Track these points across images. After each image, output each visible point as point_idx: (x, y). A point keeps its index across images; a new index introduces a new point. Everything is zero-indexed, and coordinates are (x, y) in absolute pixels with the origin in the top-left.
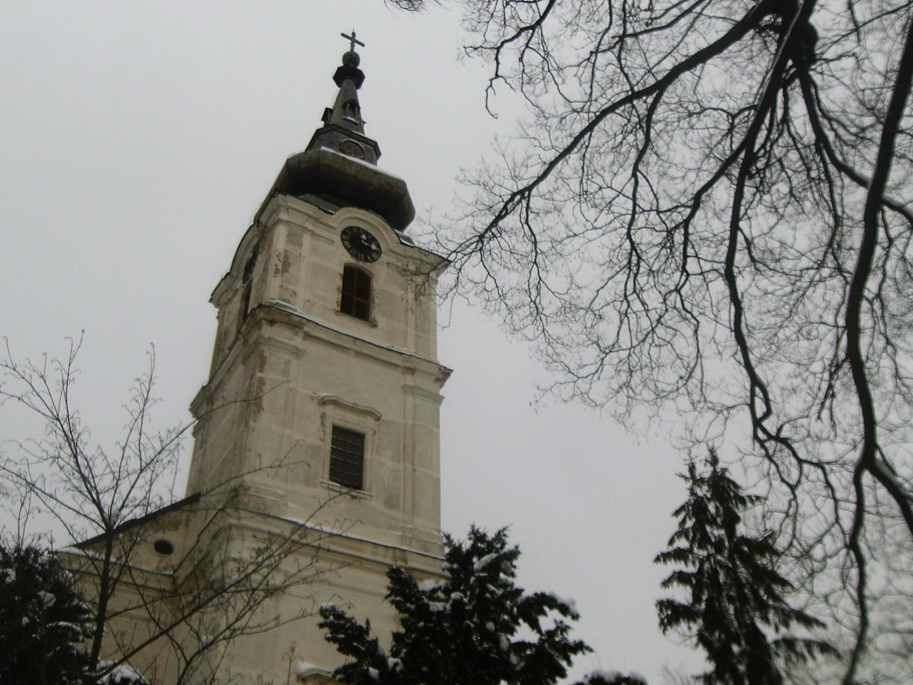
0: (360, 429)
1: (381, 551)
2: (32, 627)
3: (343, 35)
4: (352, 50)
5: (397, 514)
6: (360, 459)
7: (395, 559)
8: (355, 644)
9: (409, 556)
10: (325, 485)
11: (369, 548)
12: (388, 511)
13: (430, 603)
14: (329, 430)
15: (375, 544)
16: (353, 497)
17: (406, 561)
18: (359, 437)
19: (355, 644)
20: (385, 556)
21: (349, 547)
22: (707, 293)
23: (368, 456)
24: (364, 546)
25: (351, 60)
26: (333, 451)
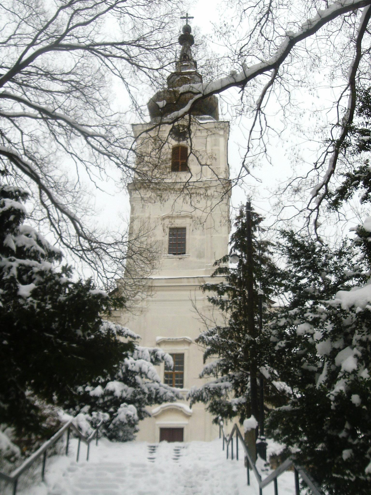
0: (183, 226)
1: (192, 280)
2: (220, 351)
3: (193, 18)
4: (187, 24)
5: (203, 260)
6: (184, 239)
7: (199, 282)
8: (9, 334)
9: (205, 279)
10: (166, 257)
11: (186, 280)
12: (198, 260)
13: (263, 294)
14: (167, 230)
15: (187, 278)
16: (180, 259)
17: (205, 282)
18: (184, 229)
19: (9, 334)
20: (194, 282)
21: (177, 282)
22: (92, 127)
23: (187, 237)
24: (183, 280)
25: (187, 29)
26: (170, 240)
